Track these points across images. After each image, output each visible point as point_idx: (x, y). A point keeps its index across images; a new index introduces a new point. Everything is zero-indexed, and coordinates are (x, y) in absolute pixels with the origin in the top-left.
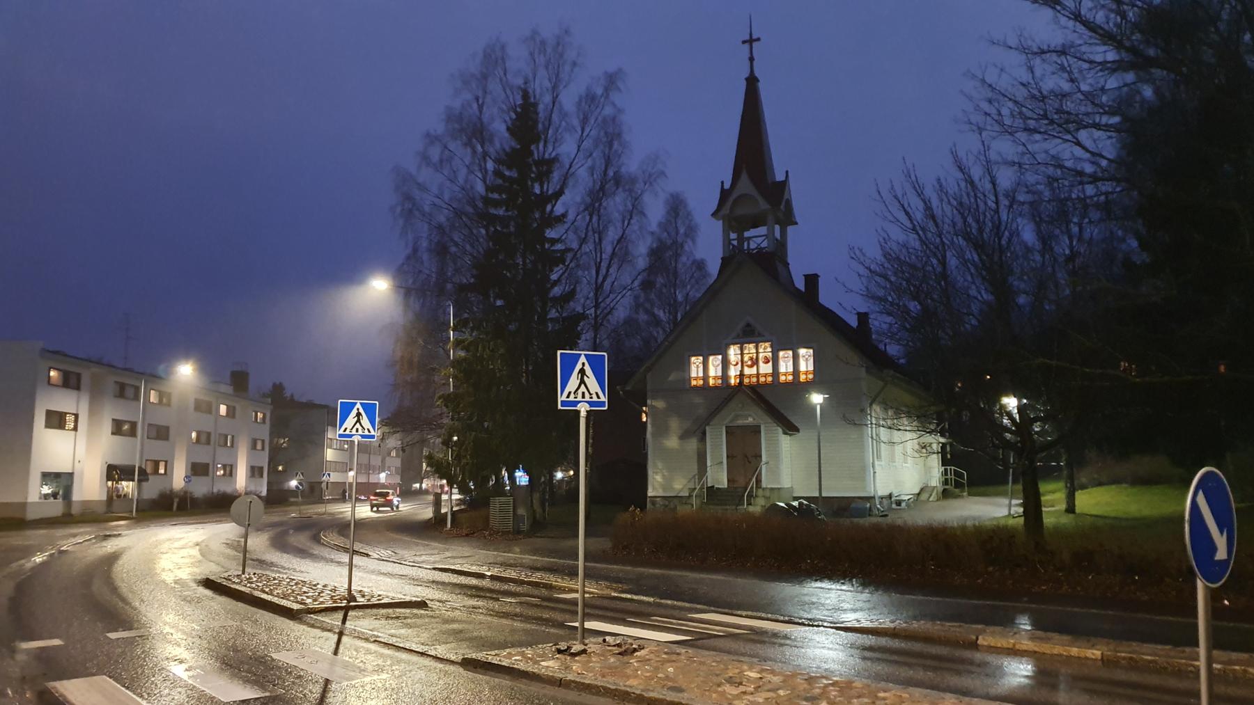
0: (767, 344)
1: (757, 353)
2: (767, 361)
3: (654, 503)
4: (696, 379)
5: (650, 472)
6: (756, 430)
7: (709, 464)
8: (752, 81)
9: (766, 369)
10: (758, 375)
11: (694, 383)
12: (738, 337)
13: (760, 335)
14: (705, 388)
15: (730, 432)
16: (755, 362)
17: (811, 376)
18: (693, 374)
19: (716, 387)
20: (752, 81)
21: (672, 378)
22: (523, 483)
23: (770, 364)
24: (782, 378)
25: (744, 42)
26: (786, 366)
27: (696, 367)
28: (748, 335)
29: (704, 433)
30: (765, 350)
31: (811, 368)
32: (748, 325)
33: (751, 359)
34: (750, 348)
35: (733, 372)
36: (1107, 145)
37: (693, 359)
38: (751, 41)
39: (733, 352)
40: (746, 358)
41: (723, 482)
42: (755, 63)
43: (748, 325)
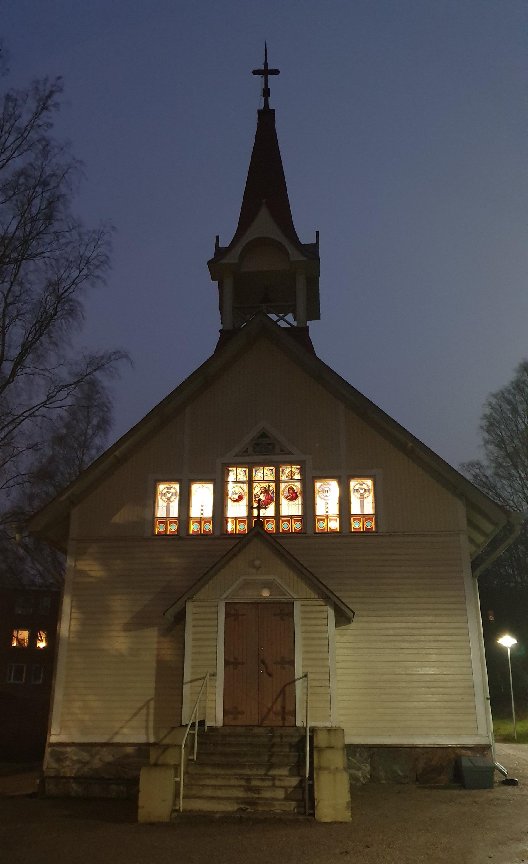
0: (295, 469)
1: (278, 481)
2: (293, 497)
3: (59, 758)
4: (165, 521)
5: (59, 695)
6: (284, 612)
7: (187, 677)
8: (266, 118)
9: (291, 508)
10: (278, 516)
11: (160, 529)
12: (245, 453)
13: (283, 452)
14: (183, 536)
15: (233, 612)
16: (273, 497)
17: (270, 527)
18: (161, 513)
19: (199, 536)
20: (266, 118)
21: (119, 518)
22: (38, 645)
23: (299, 501)
24: (194, 527)
25: (256, 72)
26: (202, 497)
27: (166, 503)
28: (263, 451)
29: (180, 617)
30: (291, 474)
31: (369, 509)
32: (264, 435)
33: (266, 491)
34: (263, 474)
35: (236, 510)
36: (299, 724)
37: (162, 487)
38: (265, 72)
39: (236, 476)
40: (257, 490)
41: (216, 717)
42: (270, 99)
43: (264, 435)
